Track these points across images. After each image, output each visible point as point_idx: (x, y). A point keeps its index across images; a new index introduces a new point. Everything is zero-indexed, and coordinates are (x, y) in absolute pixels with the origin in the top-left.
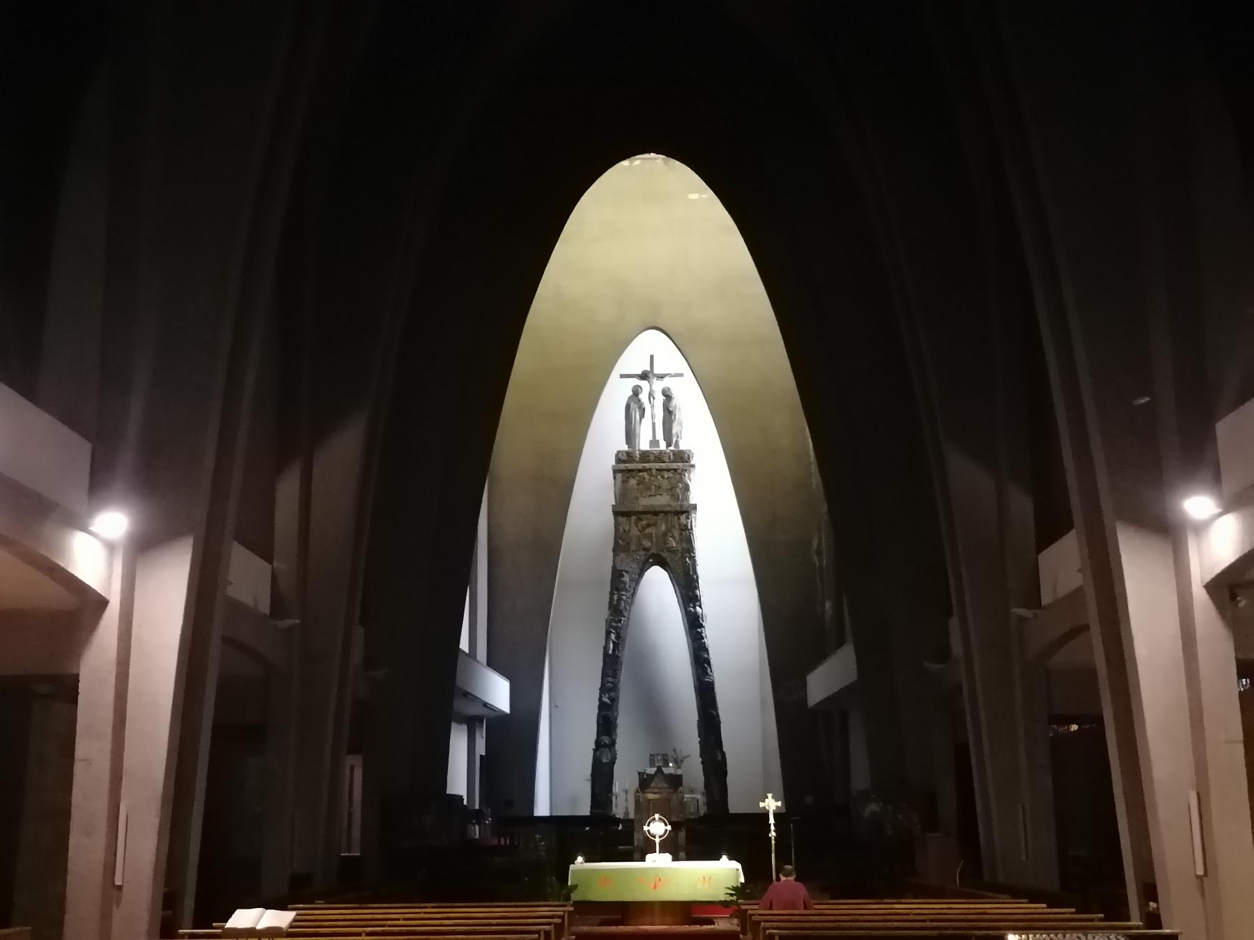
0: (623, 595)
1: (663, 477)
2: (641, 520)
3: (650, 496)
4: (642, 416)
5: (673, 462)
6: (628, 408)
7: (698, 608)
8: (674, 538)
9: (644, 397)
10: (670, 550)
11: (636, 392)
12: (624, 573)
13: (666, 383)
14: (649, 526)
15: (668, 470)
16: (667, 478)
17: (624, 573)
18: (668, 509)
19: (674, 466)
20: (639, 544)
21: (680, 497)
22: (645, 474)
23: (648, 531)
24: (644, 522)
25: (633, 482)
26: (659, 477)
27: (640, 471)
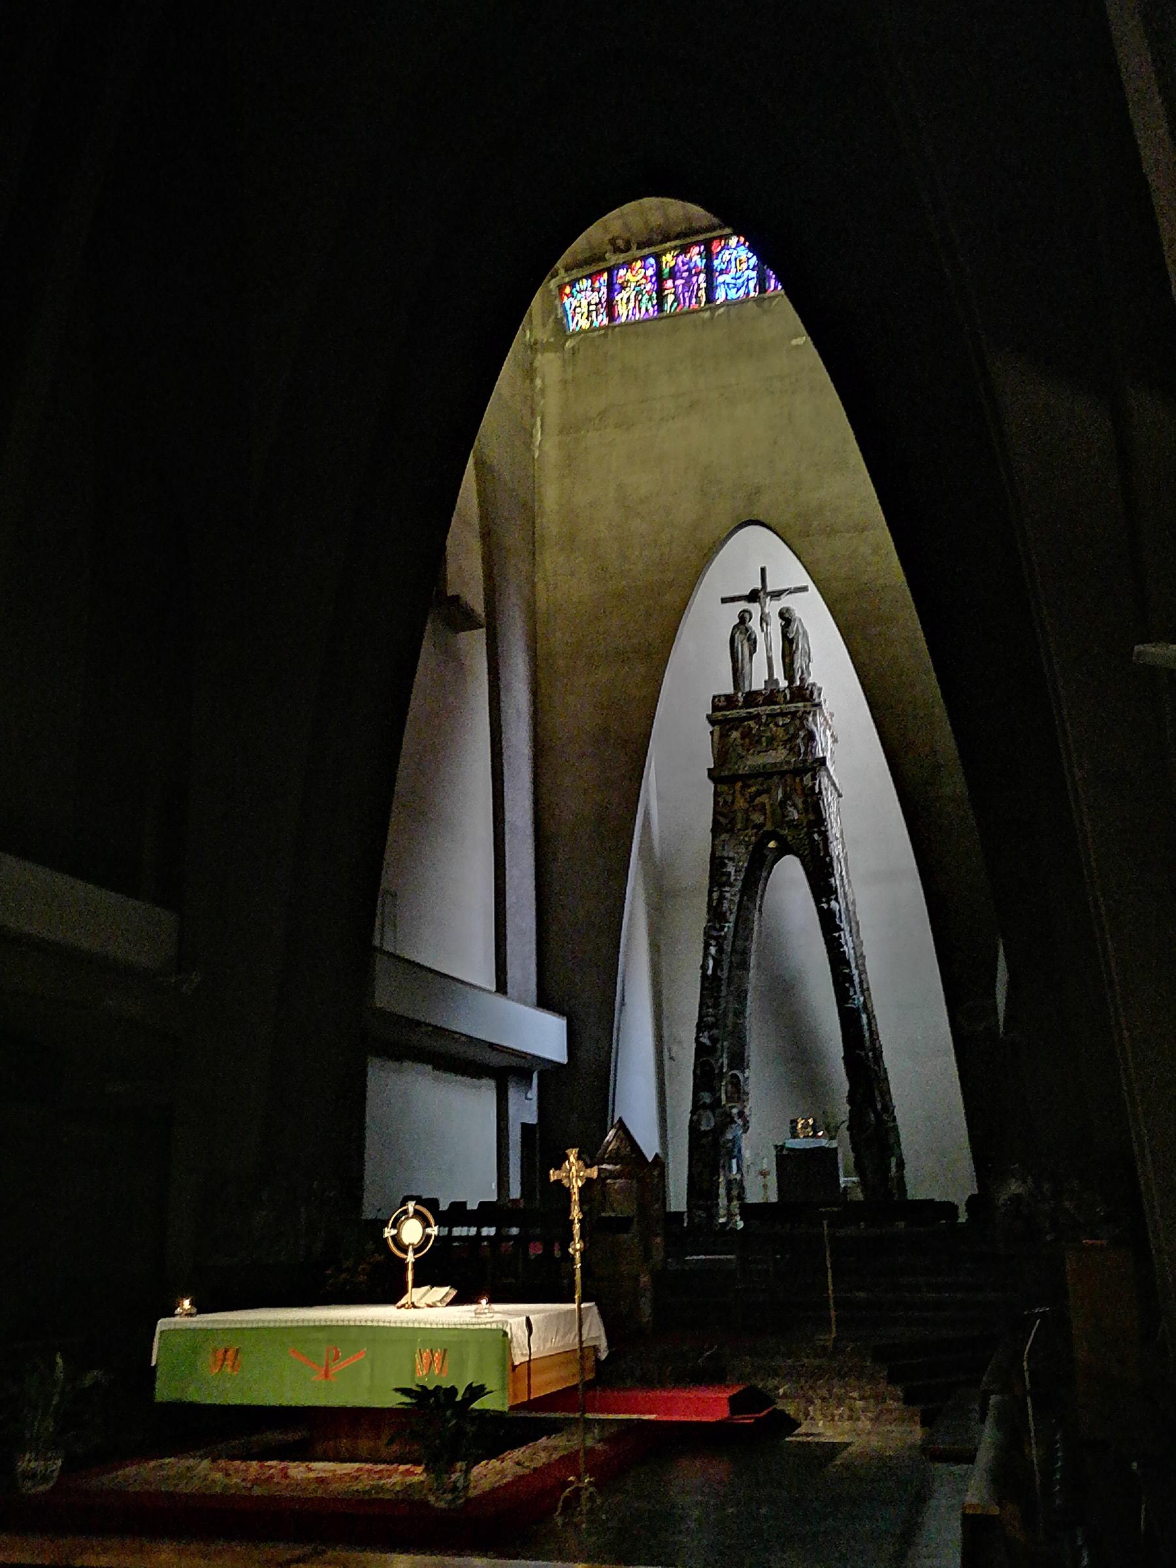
0: (727, 892)
2: (749, 786)
4: (753, 650)
5: (791, 701)
6: (810, 661)
7: (833, 903)
8: (795, 806)
9: (754, 624)
10: (791, 825)
11: (743, 618)
12: (726, 861)
13: (785, 601)
14: (759, 793)
15: (783, 714)
16: (783, 725)
17: (726, 861)
19: (792, 707)
20: (748, 820)
21: (802, 751)
22: (752, 723)
23: (758, 800)
25: (735, 734)
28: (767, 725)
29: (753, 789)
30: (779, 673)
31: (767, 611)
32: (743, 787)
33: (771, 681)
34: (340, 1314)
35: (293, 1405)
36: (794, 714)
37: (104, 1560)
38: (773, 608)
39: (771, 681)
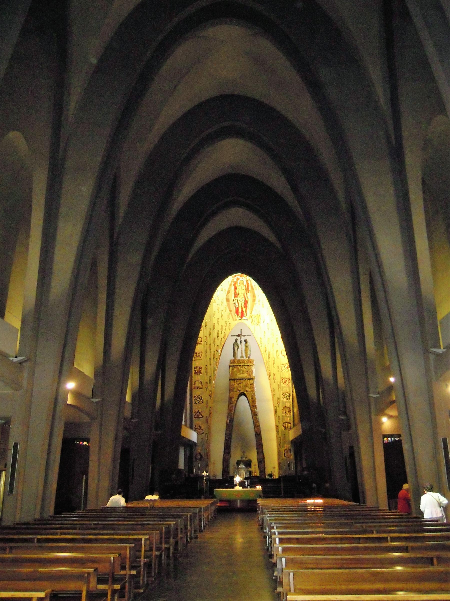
4: (238, 348)
9: (239, 342)
11: (236, 340)
13: (246, 338)
18: (246, 378)
23: (240, 385)
24: (239, 382)
25: (235, 369)
26: (244, 368)
27: (237, 366)
28: (242, 368)
30: (244, 354)
32: (237, 382)
35: (355, 455)
36: (248, 366)
37: (161, 600)
38: (243, 339)
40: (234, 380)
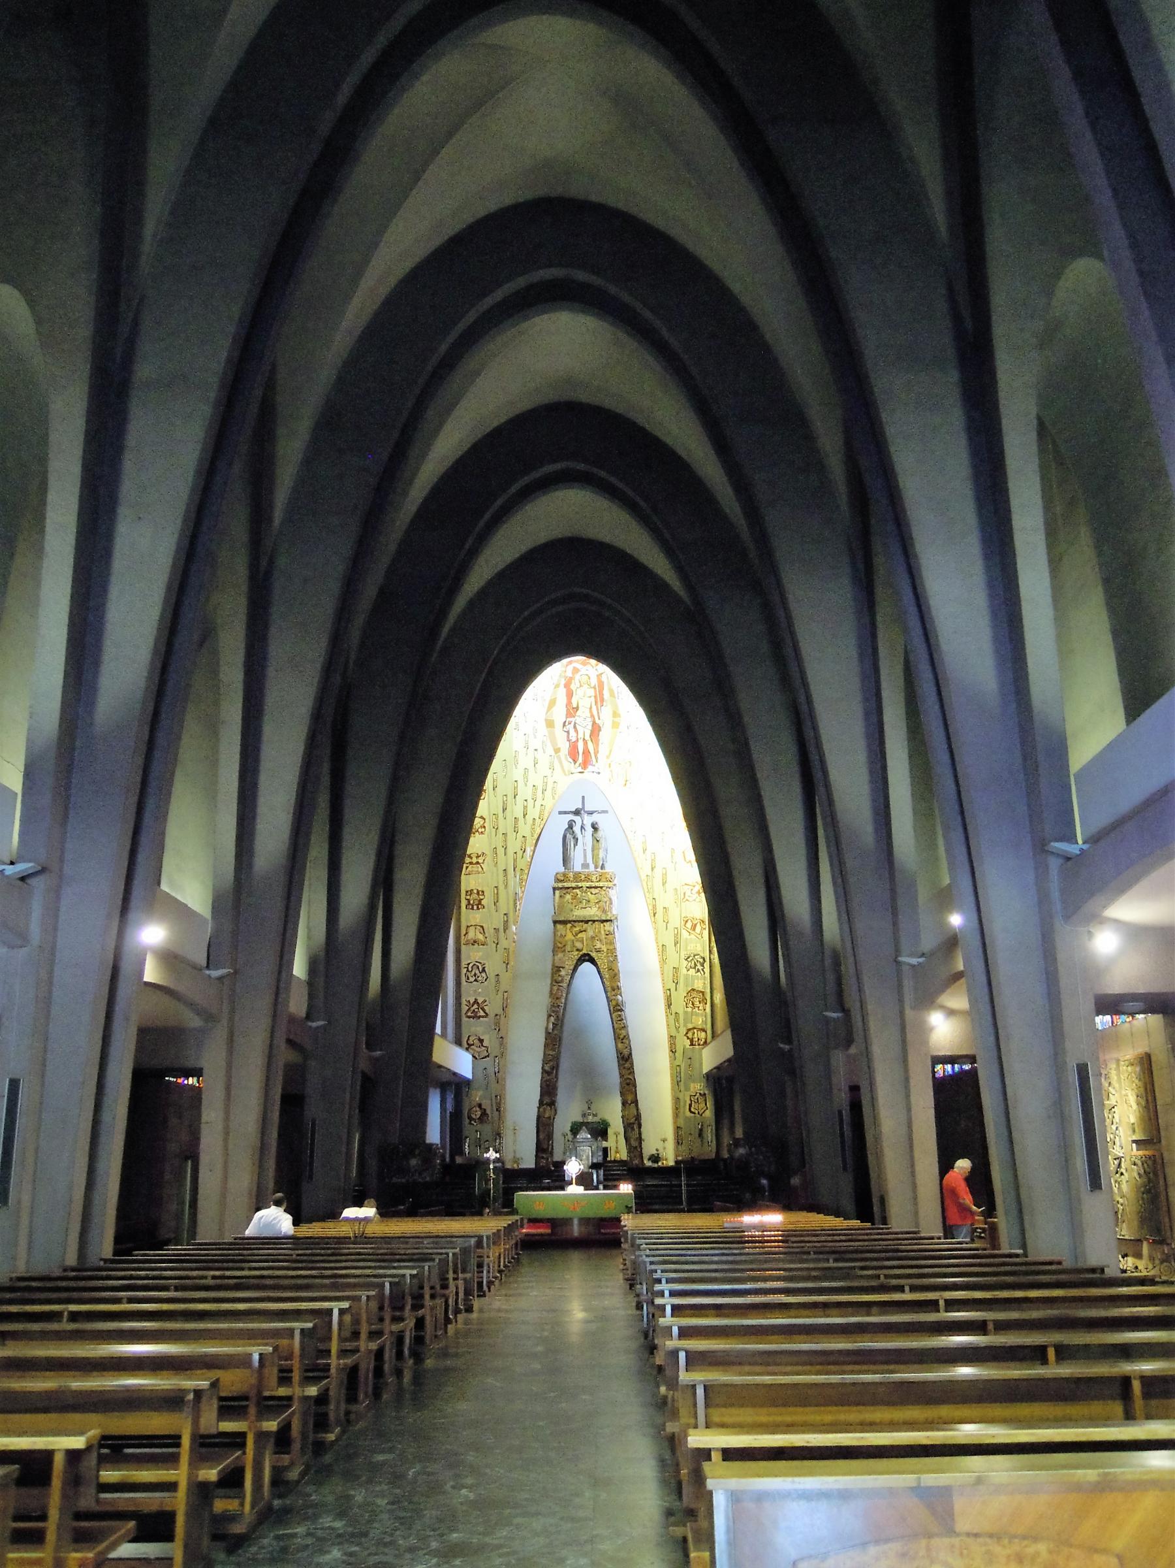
1: (592, 893)
3: (582, 908)
4: (576, 844)
6: (565, 837)
9: (577, 829)
11: (571, 826)
18: (596, 918)
22: (578, 891)
23: (580, 935)
25: (568, 897)
27: (574, 888)
28: (586, 892)
29: (577, 929)
30: (589, 860)
31: (585, 822)
33: (585, 865)
34: (94, 1326)
36: (601, 887)
38: (588, 821)
39: (585, 865)
40: (564, 922)
